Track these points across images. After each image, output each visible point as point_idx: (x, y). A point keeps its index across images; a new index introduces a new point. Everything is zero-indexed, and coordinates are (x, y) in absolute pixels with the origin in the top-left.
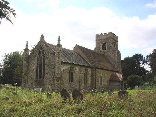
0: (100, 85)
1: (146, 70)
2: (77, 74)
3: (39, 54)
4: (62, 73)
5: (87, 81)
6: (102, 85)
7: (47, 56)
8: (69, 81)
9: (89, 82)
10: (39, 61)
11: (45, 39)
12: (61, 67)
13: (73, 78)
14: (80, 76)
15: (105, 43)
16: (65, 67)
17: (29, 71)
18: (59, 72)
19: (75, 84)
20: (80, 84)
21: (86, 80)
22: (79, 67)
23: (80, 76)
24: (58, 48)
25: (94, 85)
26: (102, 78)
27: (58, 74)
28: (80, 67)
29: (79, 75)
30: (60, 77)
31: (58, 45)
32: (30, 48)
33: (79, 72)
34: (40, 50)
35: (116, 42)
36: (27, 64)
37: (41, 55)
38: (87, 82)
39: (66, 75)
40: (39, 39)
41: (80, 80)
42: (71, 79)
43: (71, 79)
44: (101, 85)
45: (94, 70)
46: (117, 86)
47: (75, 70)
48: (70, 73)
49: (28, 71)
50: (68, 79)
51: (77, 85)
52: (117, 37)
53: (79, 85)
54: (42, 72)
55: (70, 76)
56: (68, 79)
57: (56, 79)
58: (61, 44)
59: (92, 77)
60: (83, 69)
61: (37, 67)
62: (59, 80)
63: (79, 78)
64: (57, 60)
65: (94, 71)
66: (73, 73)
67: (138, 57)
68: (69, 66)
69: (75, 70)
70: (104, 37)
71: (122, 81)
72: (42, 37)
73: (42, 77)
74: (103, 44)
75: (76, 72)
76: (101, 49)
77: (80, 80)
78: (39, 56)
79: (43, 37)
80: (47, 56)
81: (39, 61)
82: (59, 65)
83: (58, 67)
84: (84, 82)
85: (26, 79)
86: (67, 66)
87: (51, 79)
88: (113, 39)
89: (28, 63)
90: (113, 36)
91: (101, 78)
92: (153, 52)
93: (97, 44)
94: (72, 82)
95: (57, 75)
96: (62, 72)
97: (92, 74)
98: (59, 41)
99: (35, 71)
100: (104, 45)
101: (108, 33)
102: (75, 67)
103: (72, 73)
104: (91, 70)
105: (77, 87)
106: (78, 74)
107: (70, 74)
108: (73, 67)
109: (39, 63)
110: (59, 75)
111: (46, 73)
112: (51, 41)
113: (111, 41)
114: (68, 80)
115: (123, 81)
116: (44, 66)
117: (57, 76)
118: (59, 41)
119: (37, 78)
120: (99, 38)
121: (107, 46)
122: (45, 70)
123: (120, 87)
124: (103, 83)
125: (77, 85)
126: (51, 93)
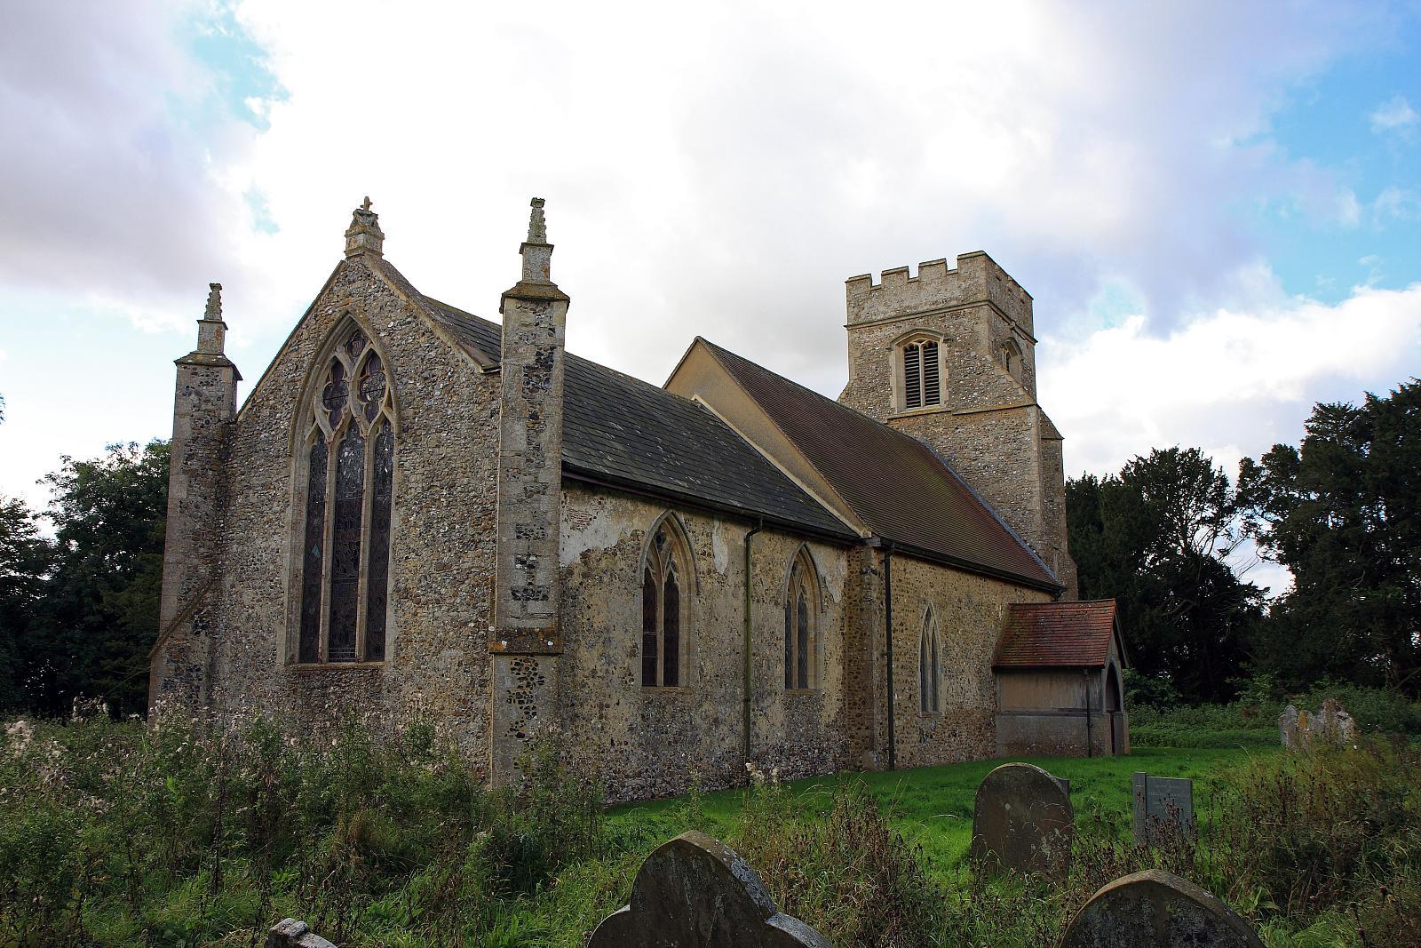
0: (924, 708)
1: (1294, 576)
2: (720, 601)
3: (333, 398)
4: (567, 592)
5: (810, 672)
6: (942, 707)
7: (410, 412)
8: (649, 678)
9: (829, 679)
10: (330, 477)
11: (391, 252)
12: (565, 528)
13: (682, 650)
14: (747, 621)
15: (931, 348)
16: (604, 528)
17: (229, 579)
18: (542, 578)
19: (706, 706)
20: (747, 701)
21: (798, 672)
22: (738, 534)
23: (747, 621)
24: (530, 318)
25: (878, 704)
26: (941, 646)
27: (529, 594)
28: (747, 540)
29: (741, 610)
30: (548, 634)
31: (525, 292)
32: (252, 350)
33: (741, 578)
34: (342, 356)
35: (1023, 343)
36: (208, 507)
37: (352, 405)
38: (811, 686)
39: (617, 614)
40: (334, 252)
41: (747, 660)
42: (661, 656)
43: (661, 656)
44: (935, 707)
45: (875, 561)
46: (1069, 712)
47: (703, 565)
48: (649, 588)
49: (216, 578)
50: (632, 654)
51: (724, 711)
52: (1027, 299)
53: (740, 707)
54: (363, 583)
55: (649, 623)
56: (632, 654)
57: (507, 653)
58: (562, 274)
59: (855, 636)
60: (775, 552)
61: (313, 535)
62: (547, 667)
63: (740, 642)
64: (522, 445)
65: (875, 579)
66: (683, 596)
67: (1172, 477)
68: (646, 519)
69: (703, 565)
70: (922, 300)
71: (1112, 665)
72: (365, 224)
73: (360, 633)
74: (910, 351)
75: (708, 584)
76: (896, 401)
77: (747, 660)
78: (333, 423)
79: (374, 224)
80: (410, 412)
81: (330, 477)
82: (545, 503)
83: (525, 518)
84: (788, 684)
85: (200, 658)
86: (618, 514)
87: (451, 655)
88: (999, 311)
89: (223, 498)
90: (996, 290)
91: (928, 643)
92: (1310, 430)
93: (862, 360)
94: (671, 678)
95: (515, 606)
96: (576, 580)
97: (855, 608)
98: (537, 246)
99: (284, 577)
100: (919, 359)
101: (952, 265)
102: (696, 527)
103: (671, 587)
104: (844, 563)
105: (724, 729)
106: (729, 605)
107: (649, 604)
108: (679, 532)
109: (329, 491)
110: (534, 607)
111: (405, 594)
112: (463, 271)
113: (981, 326)
114: (636, 666)
115: (1118, 665)
116: (381, 522)
117: (515, 623)
118: (537, 246)
119: (307, 652)
120: (880, 310)
121: (943, 374)
122: (391, 567)
123: (1095, 719)
124: (944, 685)
125: (724, 711)
126: (704, 825)
